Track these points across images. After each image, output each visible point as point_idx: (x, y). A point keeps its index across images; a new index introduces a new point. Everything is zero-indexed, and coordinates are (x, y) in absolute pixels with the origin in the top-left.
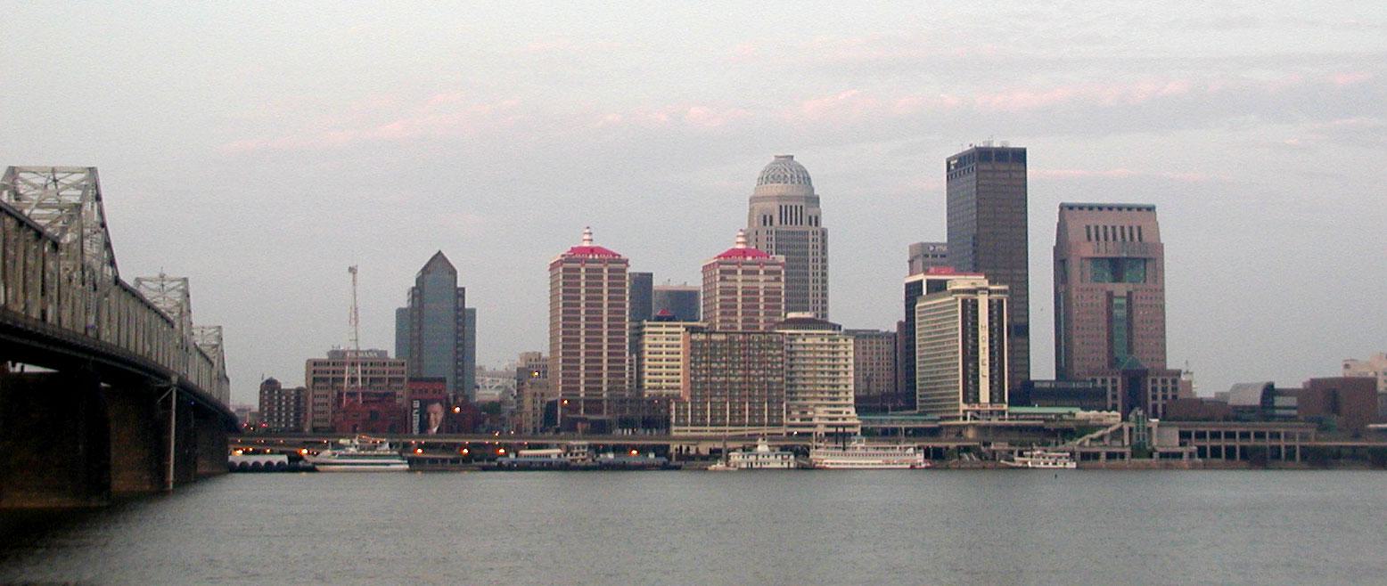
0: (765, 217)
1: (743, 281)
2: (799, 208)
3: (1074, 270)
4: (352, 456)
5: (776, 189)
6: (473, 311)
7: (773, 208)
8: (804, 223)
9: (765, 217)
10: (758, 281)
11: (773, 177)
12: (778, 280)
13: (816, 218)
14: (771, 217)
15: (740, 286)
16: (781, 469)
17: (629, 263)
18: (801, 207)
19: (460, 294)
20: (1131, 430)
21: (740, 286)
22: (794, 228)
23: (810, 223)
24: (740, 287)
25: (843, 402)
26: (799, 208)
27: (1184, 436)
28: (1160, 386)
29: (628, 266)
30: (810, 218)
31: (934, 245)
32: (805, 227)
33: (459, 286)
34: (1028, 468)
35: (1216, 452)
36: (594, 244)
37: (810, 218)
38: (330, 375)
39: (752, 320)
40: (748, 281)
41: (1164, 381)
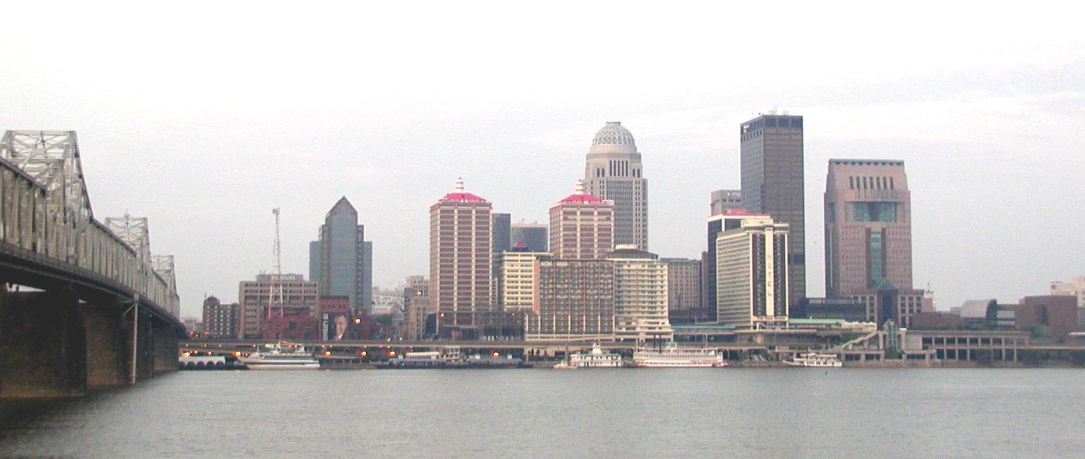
0: (598, 170)
1: (581, 220)
2: (625, 163)
3: (840, 212)
4: (275, 357)
5: (607, 148)
6: (370, 244)
7: (605, 163)
8: (629, 174)
9: (598, 170)
10: (593, 220)
11: (605, 138)
12: (609, 219)
13: (639, 171)
14: (603, 170)
15: (579, 224)
16: (611, 367)
17: (492, 206)
18: (627, 162)
19: (360, 230)
20: (885, 336)
21: (579, 224)
22: (621, 178)
23: (634, 175)
24: (579, 225)
25: (659, 315)
26: (625, 163)
27: (927, 341)
28: (907, 302)
29: (491, 208)
30: (634, 171)
31: (731, 192)
32: (630, 177)
33: (359, 223)
34: (804, 366)
35: (951, 354)
36: (465, 191)
37: (634, 171)
38: (258, 294)
39: (588, 251)
40: (585, 220)
41: (911, 299)
